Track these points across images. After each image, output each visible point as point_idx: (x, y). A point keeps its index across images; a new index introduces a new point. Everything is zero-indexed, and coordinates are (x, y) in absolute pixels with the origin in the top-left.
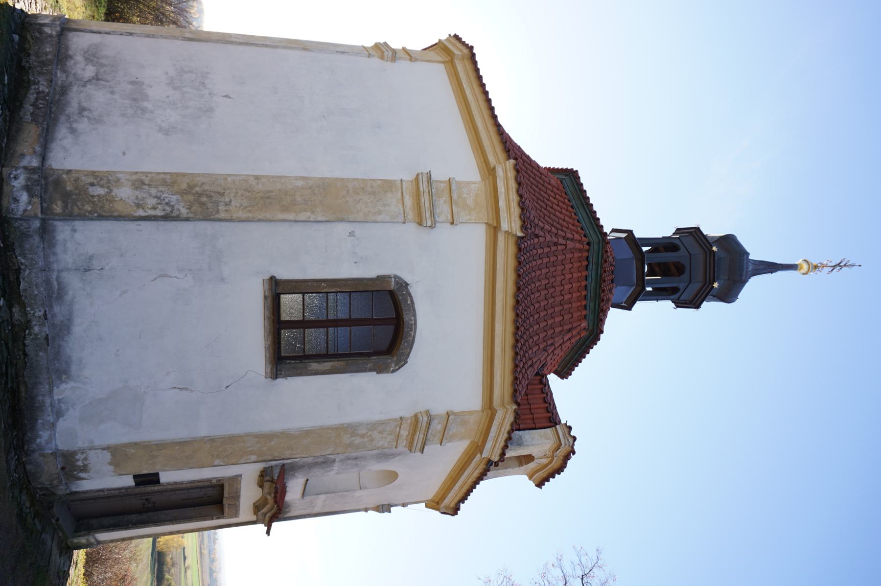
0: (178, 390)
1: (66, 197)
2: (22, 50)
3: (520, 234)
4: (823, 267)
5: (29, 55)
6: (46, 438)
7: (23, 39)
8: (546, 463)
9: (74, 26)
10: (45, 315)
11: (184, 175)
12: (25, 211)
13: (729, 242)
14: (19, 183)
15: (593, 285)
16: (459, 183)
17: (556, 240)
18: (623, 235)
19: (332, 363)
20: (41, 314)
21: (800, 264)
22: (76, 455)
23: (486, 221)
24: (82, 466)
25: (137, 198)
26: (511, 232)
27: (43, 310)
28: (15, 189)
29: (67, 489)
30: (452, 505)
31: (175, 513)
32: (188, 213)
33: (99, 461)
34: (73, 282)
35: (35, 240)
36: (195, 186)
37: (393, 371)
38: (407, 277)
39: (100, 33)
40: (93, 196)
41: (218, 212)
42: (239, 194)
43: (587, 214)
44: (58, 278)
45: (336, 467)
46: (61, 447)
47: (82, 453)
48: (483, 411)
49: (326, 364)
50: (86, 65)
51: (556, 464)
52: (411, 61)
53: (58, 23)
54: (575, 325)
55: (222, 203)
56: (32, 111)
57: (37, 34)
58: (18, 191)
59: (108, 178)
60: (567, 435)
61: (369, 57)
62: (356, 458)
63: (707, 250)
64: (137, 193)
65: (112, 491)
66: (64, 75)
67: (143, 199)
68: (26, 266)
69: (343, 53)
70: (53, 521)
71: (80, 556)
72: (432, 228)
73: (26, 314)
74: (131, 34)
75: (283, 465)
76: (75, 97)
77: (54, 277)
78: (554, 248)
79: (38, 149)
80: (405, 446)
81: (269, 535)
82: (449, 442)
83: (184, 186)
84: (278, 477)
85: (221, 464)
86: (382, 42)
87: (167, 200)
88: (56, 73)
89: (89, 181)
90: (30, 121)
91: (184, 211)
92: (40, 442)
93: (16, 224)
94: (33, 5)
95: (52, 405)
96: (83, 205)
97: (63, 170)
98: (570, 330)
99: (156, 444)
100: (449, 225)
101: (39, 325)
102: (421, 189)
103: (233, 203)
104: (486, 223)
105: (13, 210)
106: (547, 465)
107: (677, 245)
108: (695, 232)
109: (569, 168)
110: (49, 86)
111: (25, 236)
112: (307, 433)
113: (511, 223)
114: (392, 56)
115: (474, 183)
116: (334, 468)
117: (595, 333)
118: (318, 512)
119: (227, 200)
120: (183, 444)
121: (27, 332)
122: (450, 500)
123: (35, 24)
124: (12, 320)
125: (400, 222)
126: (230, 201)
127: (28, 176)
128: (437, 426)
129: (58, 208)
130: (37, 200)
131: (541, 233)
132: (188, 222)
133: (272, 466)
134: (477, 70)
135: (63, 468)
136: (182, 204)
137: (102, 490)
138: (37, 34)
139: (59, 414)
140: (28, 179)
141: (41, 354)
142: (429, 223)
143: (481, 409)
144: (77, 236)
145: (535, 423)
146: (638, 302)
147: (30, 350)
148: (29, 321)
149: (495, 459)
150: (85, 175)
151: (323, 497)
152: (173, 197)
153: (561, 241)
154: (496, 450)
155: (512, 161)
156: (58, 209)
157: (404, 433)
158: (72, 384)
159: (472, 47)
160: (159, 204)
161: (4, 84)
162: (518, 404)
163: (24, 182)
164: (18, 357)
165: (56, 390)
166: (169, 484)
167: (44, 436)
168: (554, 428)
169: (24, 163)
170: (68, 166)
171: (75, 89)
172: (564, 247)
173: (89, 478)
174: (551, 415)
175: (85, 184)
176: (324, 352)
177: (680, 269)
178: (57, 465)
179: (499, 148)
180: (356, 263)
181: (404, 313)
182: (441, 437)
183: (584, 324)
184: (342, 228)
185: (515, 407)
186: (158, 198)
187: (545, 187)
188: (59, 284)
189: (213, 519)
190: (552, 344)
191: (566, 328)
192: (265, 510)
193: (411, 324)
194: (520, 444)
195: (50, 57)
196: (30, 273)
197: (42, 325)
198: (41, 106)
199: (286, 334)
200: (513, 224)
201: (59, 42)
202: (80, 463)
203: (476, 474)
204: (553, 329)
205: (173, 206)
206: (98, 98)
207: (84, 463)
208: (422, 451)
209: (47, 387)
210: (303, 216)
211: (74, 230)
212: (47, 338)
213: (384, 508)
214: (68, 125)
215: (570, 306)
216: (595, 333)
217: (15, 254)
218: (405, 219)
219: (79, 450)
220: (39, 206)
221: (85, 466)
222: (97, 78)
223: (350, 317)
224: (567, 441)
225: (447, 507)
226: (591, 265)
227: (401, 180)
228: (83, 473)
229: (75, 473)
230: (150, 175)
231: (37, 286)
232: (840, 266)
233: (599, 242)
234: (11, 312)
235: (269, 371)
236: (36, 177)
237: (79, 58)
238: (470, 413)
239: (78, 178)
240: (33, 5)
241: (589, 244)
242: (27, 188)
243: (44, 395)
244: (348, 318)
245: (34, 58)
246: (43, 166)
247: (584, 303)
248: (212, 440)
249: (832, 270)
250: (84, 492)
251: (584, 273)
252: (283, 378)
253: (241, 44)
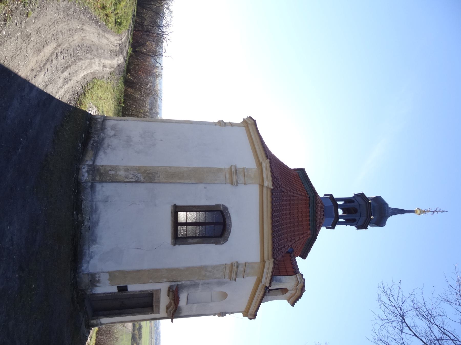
0: (137, 249)
1: (101, 174)
2: (90, 126)
3: (272, 188)
4: (428, 212)
5: (92, 128)
6: (85, 267)
7: (90, 123)
8: (294, 293)
9: (108, 118)
10: (90, 218)
11: (143, 167)
12: (86, 179)
13: (378, 200)
14: (84, 170)
15: (312, 215)
16: (247, 169)
17: (293, 195)
18: (328, 196)
19: (197, 240)
20: (88, 218)
21: (416, 210)
22: (96, 275)
23: (259, 183)
24: (98, 280)
25: (126, 175)
26: (268, 187)
27: (89, 216)
28: (83, 172)
29: (91, 292)
30: (253, 313)
31: (134, 310)
32: (144, 180)
33: (104, 278)
34: (101, 206)
35: (88, 190)
36: (147, 170)
37: (222, 244)
38: (227, 205)
39: (117, 120)
40: (110, 174)
41: (155, 180)
42: (163, 173)
43: (308, 185)
44: (95, 204)
45: (200, 287)
46: (90, 271)
47: (98, 274)
48: (260, 262)
49: (195, 240)
50: (111, 131)
51: (298, 293)
52: (231, 126)
53: (103, 117)
54: (305, 232)
55: (157, 177)
56: (91, 146)
57: (95, 122)
58: (84, 173)
59: (116, 168)
60: (301, 278)
61: (215, 125)
62: (208, 284)
63: (367, 202)
64: (126, 173)
65: (109, 294)
66: (103, 135)
67: (128, 175)
68: (85, 199)
69: (205, 124)
70: (84, 308)
71: (94, 331)
72: (237, 186)
73: (82, 217)
74: (128, 120)
75: (178, 285)
76: (106, 142)
77: (94, 204)
78: (292, 198)
79: (92, 158)
80: (228, 278)
81: (172, 323)
82: (247, 277)
83: (143, 171)
84: (175, 290)
85: (152, 282)
86: (221, 120)
87: (136, 176)
88: (101, 134)
89: (109, 169)
90: (90, 150)
91: (142, 180)
92: (83, 269)
93: (83, 184)
94: (95, 113)
95: (89, 254)
96: (106, 177)
97: (100, 165)
98: (303, 234)
99: (127, 271)
100: (244, 185)
101: (87, 222)
102: (233, 171)
103: (161, 177)
104: (259, 184)
105: (82, 179)
106: (295, 294)
107: (353, 200)
108: (361, 195)
109: (301, 168)
110: (98, 138)
111: (86, 188)
112: (187, 269)
113: (268, 183)
114: (224, 125)
115: (254, 169)
116: (199, 288)
117: (314, 236)
118: (194, 314)
119: (159, 175)
120: (137, 272)
121: (83, 224)
122: (252, 311)
123: (95, 118)
124: (77, 220)
125: (224, 184)
126: (160, 176)
127: (88, 167)
128: (241, 269)
129: (97, 178)
130: (90, 176)
131: (285, 191)
132: (144, 184)
133: (173, 285)
134: (257, 128)
135: (90, 281)
136: (142, 177)
137: (104, 293)
138: (95, 122)
139: (91, 258)
140: (88, 169)
141: (87, 233)
142: (235, 184)
143: (259, 262)
144: (104, 189)
145: (286, 269)
146: (336, 226)
147: (83, 231)
148: (84, 220)
149: (267, 285)
150: (108, 167)
151: (195, 305)
152: (139, 174)
153: (295, 195)
154: (267, 281)
155: (269, 160)
156: (98, 179)
157: (227, 271)
158: (97, 245)
159: (255, 120)
160: (134, 177)
161: (83, 137)
162: (275, 259)
163: (87, 169)
164: (78, 234)
165: (91, 248)
166: (131, 292)
167: (85, 266)
168: (295, 275)
169: (87, 163)
170: (102, 164)
171: (107, 139)
172: (297, 198)
173: (100, 286)
174: (295, 270)
175: (108, 170)
176: (194, 236)
177: (355, 211)
178: (88, 279)
179: (264, 155)
180: (207, 199)
181: (227, 220)
182: (243, 274)
183: (309, 232)
184: (201, 186)
185: (273, 260)
186: (133, 175)
187: (290, 175)
188: (96, 206)
189: (149, 314)
190: (294, 239)
191: (300, 233)
192: (170, 309)
193: (230, 224)
194: (280, 281)
195: (99, 129)
196: (86, 202)
197: (88, 222)
198: (95, 145)
199: (179, 228)
200: (269, 184)
201: (103, 124)
202: (97, 279)
203: (261, 295)
204: (295, 232)
205: (138, 178)
206: (115, 142)
207: (98, 279)
208: (235, 280)
209: (88, 246)
210: (187, 181)
211: (103, 187)
212: (89, 227)
213: (223, 314)
214: (104, 151)
215: (302, 223)
216: (314, 236)
217: (81, 195)
218: (226, 182)
219: (97, 273)
220: (91, 178)
221: (99, 280)
222: (115, 135)
223: (205, 221)
224: (301, 281)
225: (251, 315)
226: (311, 206)
227: (225, 168)
228: (98, 283)
229: (95, 283)
230: (131, 167)
231: (88, 207)
232: (437, 211)
233: (313, 196)
234: (78, 217)
235: (172, 242)
236: (91, 168)
237: (109, 129)
238: (255, 263)
239: (106, 168)
240: (95, 113)
241: (309, 197)
242: (88, 172)
243: (86, 250)
244: (204, 222)
245: (93, 129)
246: (94, 164)
247: (309, 223)
248: (149, 270)
249: (433, 214)
250: (98, 294)
251: (308, 210)
252: (178, 245)
253: (167, 122)
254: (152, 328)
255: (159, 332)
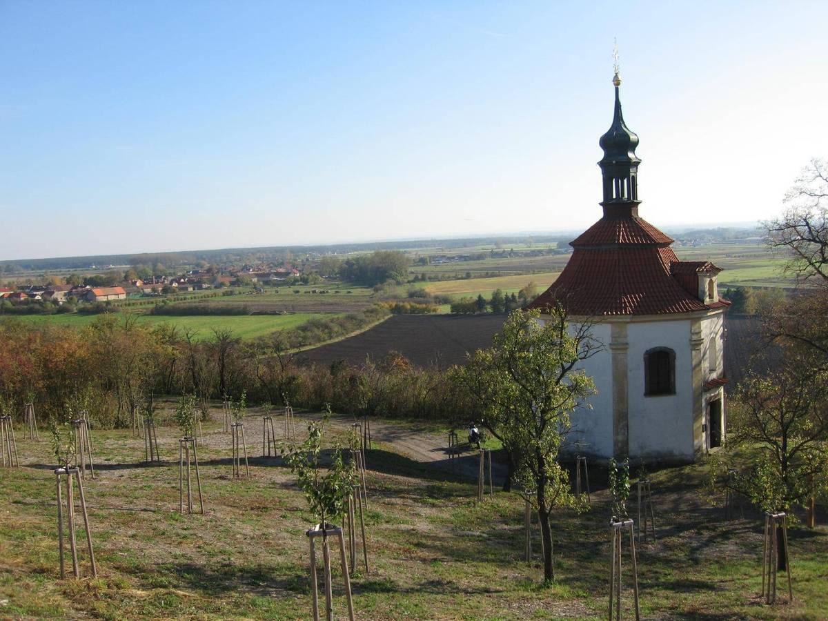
38: (644, 351)
146: (598, 214)
184: (629, 374)
254: (493, 276)
255: (686, 235)
